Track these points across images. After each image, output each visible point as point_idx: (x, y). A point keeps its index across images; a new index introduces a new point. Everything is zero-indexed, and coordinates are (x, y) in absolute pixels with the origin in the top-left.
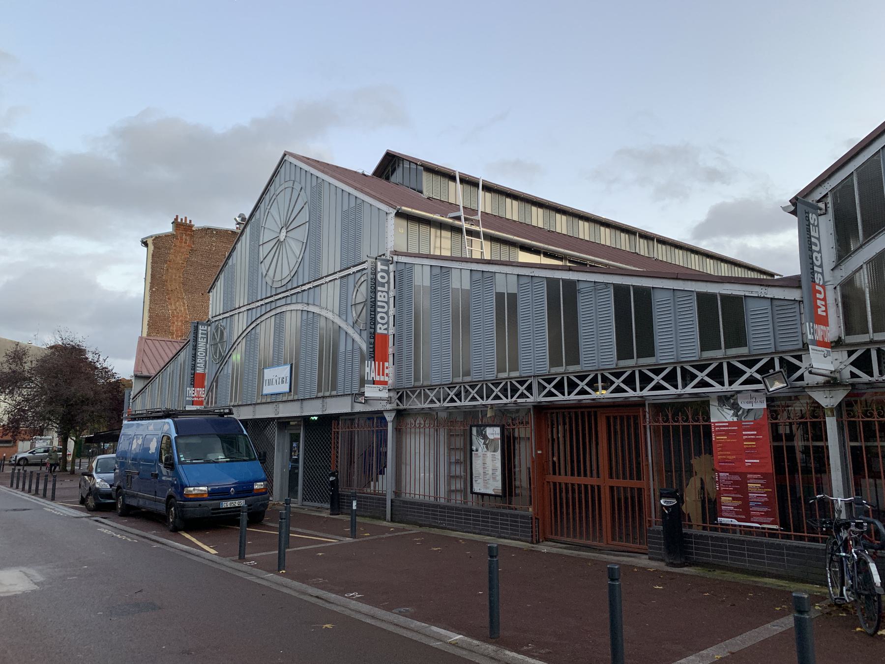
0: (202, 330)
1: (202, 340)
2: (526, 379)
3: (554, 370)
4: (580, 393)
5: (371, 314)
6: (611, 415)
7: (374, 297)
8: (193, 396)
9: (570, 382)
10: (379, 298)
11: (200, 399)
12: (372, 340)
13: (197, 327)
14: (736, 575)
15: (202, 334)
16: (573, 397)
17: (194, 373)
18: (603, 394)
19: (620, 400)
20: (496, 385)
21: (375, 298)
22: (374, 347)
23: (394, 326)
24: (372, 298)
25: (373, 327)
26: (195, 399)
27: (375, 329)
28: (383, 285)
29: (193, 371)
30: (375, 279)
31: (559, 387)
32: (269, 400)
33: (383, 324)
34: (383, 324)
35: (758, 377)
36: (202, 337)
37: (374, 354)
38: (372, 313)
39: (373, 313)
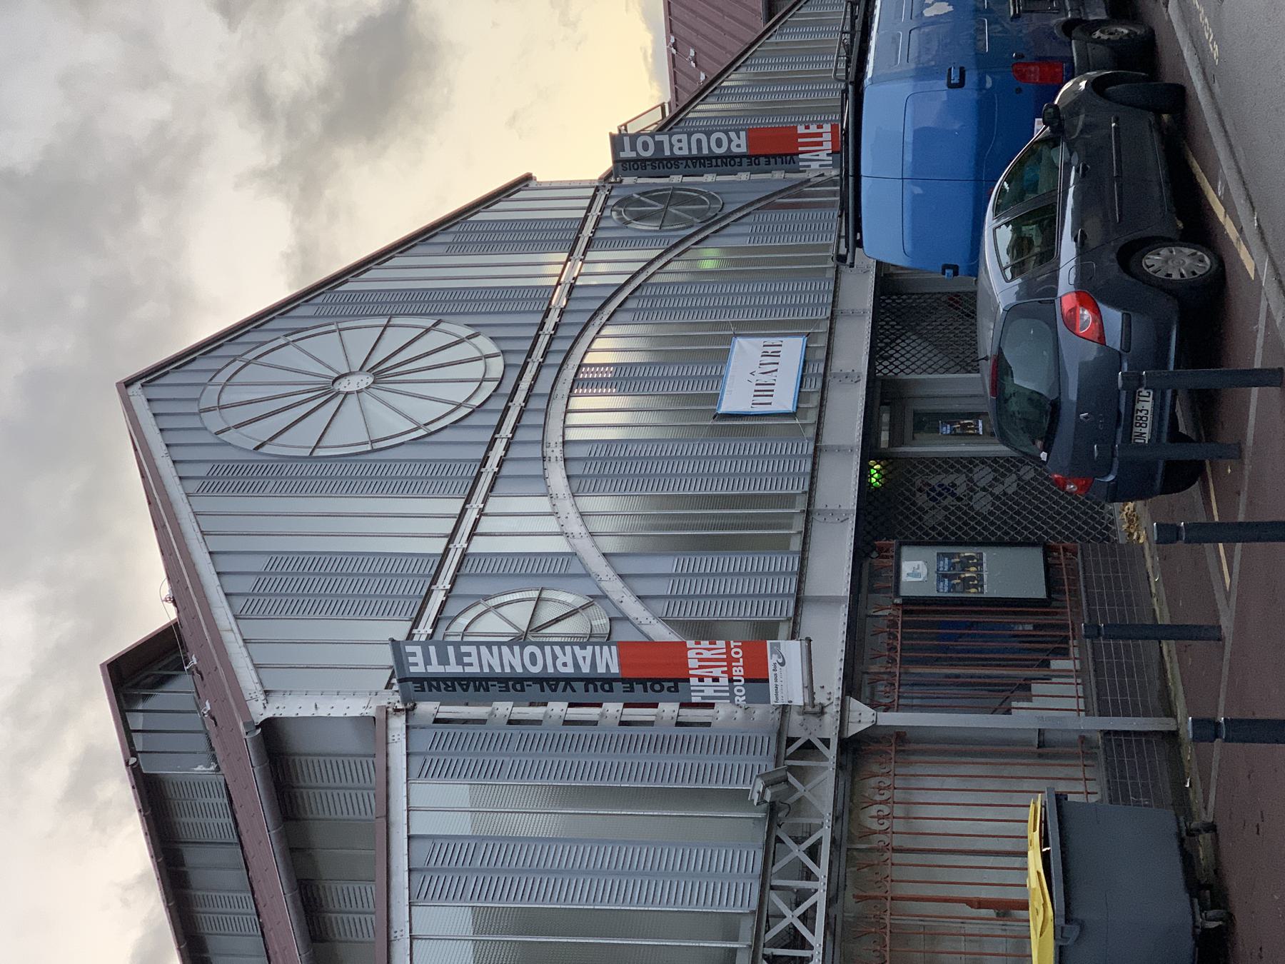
0: (427, 661)
1: (474, 659)
5: (717, 166)
7: (684, 162)
8: (724, 681)
10: (685, 152)
12: (763, 160)
15: (443, 660)
17: (623, 680)
22: (774, 156)
24: (687, 165)
26: (738, 671)
27: (741, 156)
32: (815, 400)
33: (730, 141)
34: (730, 141)
36: (459, 661)
37: (786, 155)
38: (714, 163)
39: (714, 161)
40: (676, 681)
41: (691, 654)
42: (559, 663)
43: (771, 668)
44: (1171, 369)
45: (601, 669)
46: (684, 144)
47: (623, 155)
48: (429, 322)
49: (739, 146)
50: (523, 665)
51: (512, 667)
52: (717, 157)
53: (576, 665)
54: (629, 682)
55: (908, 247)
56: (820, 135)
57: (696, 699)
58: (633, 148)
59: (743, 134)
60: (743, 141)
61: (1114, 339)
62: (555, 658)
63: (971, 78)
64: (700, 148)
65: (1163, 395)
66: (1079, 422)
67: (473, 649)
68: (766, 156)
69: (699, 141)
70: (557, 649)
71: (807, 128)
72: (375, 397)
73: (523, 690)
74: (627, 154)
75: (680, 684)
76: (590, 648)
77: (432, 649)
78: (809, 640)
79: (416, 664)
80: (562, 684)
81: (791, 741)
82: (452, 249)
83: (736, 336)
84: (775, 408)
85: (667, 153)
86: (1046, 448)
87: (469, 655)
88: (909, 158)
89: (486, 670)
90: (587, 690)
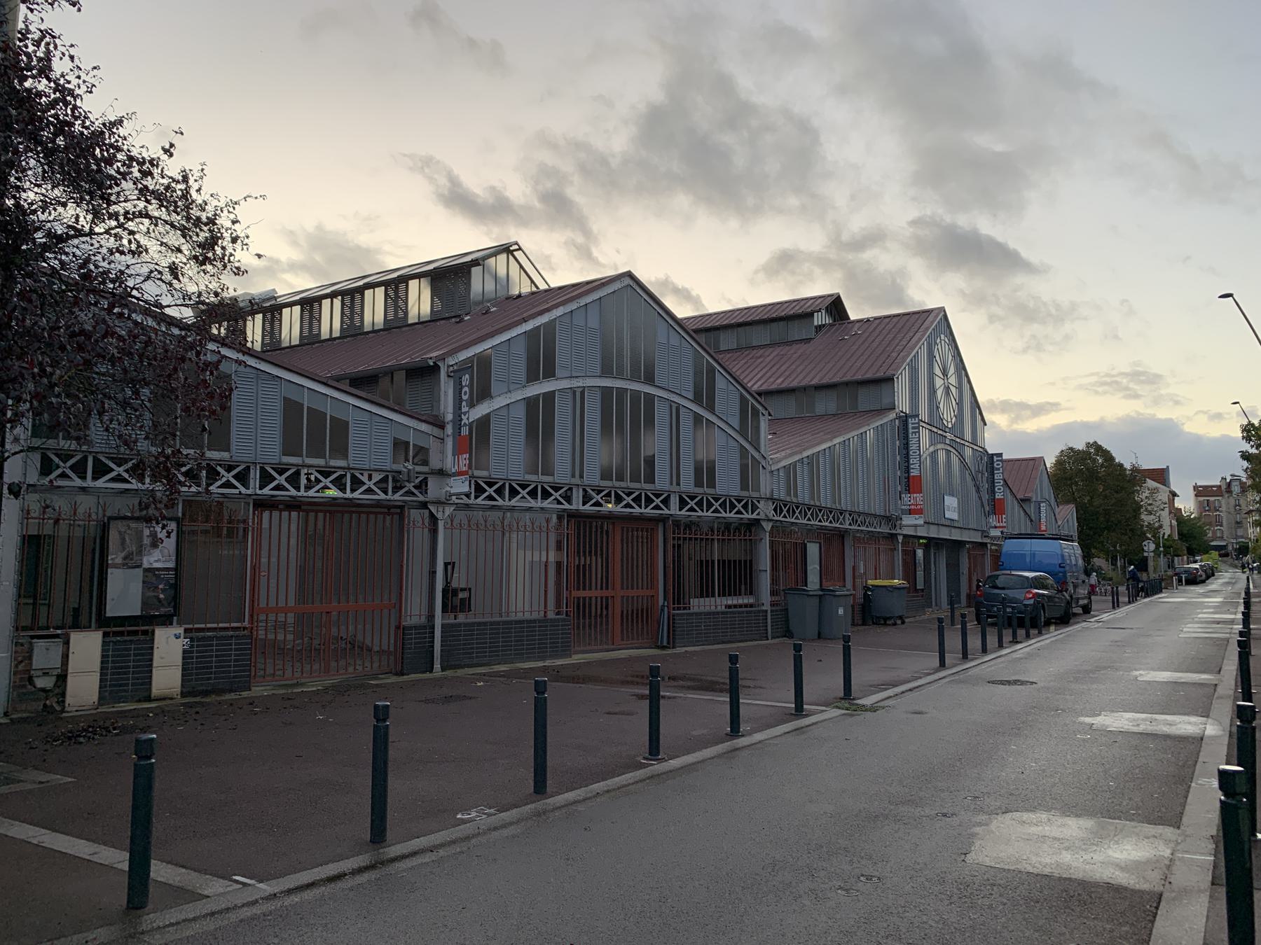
0: (912, 424)
2: (333, 470)
3: (286, 459)
4: (737, 513)
11: (919, 507)
13: (906, 421)
15: (913, 428)
16: (648, 510)
17: (908, 476)
26: (913, 507)
29: (907, 475)
31: (637, 500)
35: (126, 476)
54: (908, 478)
57: (903, 495)
58: (997, 461)
60: (1000, 497)
63: (1062, 570)
74: (995, 458)
83: (958, 499)
84: (946, 512)
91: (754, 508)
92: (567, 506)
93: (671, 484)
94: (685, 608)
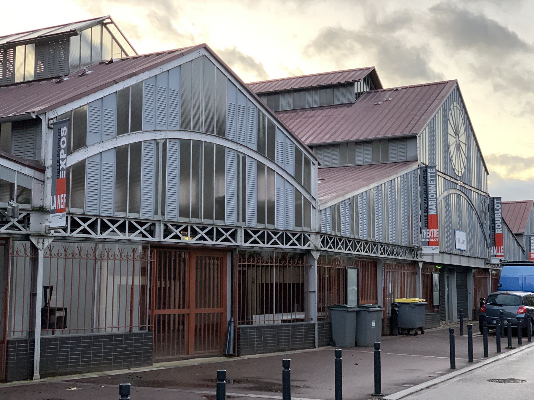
0: (431, 173)
1: (432, 183)
3: (261, 226)
6: (203, 255)
8: (428, 237)
9: (269, 236)
10: (496, 217)
14: (300, 351)
15: (431, 177)
18: (187, 239)
19: (200, 245)
20: (294, 235)
21: (494, 217)
22: (495, 240)
23: (420, 210)
25: (494, 230)
26: (430, 240)
27: (495, 231)
28: (498, 210)
29: (426, 214)
30: (494, 208)
31: (210, 234)
33: (499, 229)
34: (499, 229)
36: (431, 180)
40: (428, 226)
41: (435, 230)
42: (432, 202)
43: (432, 247)
44: (512, 327)
45: (430, 211)
46: (498, 217)
47: (495, 200)
48: (466, 156)
49: (498, 231)
50: (430, 194)
51: (430, 191)
52: (495, 225)
53: (431, 205)
55: (505, 276)
56: (501, 252)
57: (423, 230)
58: (497, 203)
59: (501, 232)
61: (519, 316)
62: (433, 201)
64: (497, 221)
65: (506, 325)
66: (499, 310)
67: (435, 183)
68: (495, 237)
69: (499, 221)
70: (435, 201)
71: (503, 249)
72: (454, 142)
73: (424, 193)
74: (496, 201)
75: (427, 227)
76: (436, 208)
77: (434, 174)
78: (439, 255)
79: (430, 170)
80: (426, 202)
81: (309, 235)
82: (477, 157)
85: (496, 212)
86: (491, 304)
87: (433, 182)
88: (511, 276)
89: (429, 186)
90: (425, 207)
91: (306, 240)
92: (150, 238)
93: (156, 213)
94: (248, 323)
